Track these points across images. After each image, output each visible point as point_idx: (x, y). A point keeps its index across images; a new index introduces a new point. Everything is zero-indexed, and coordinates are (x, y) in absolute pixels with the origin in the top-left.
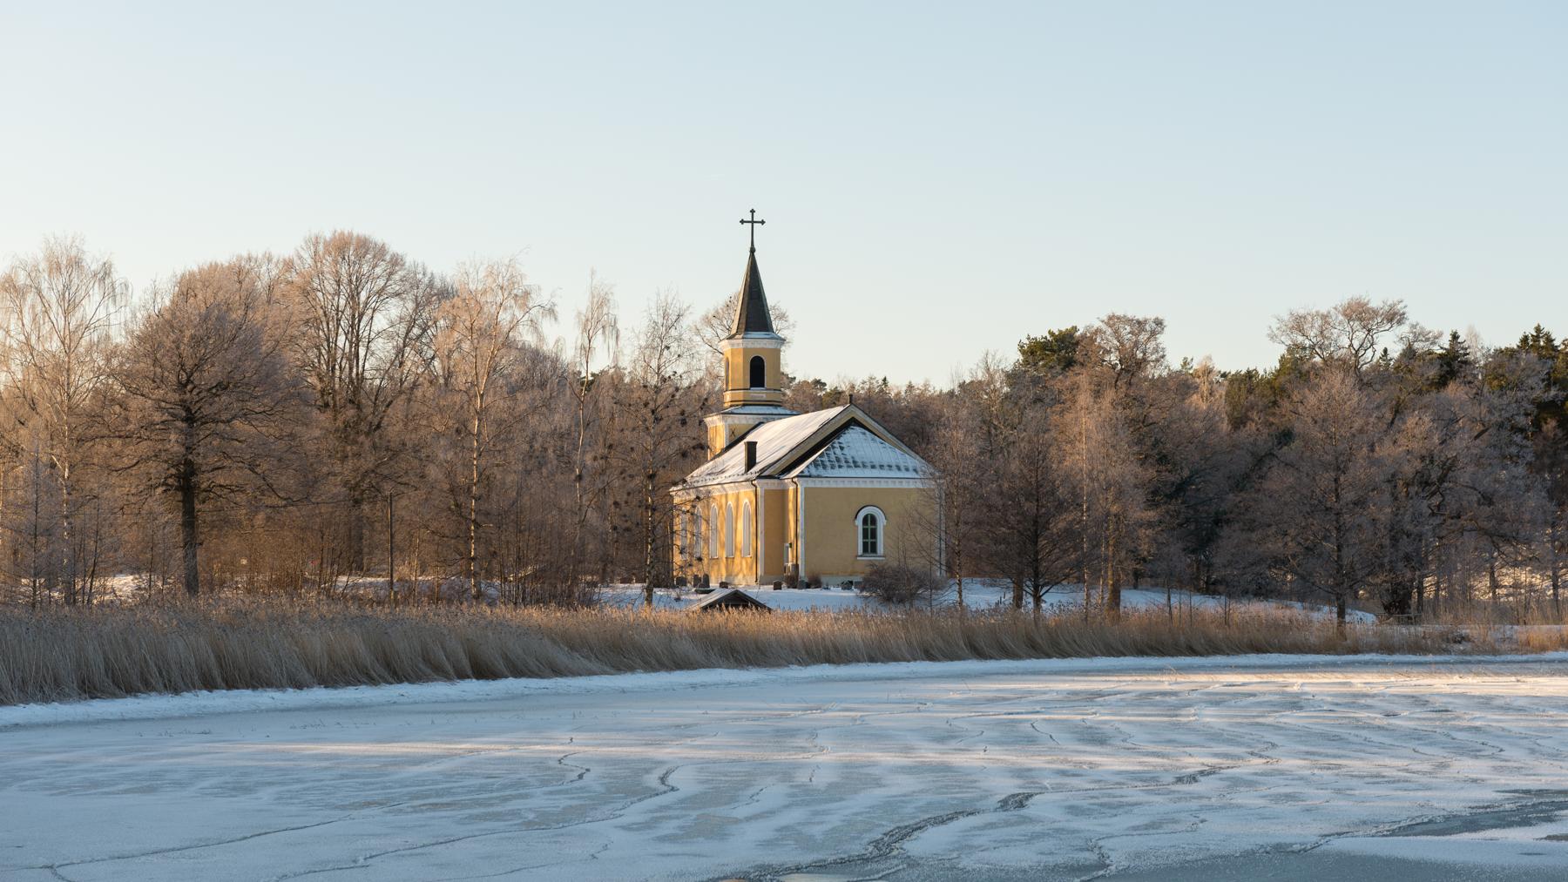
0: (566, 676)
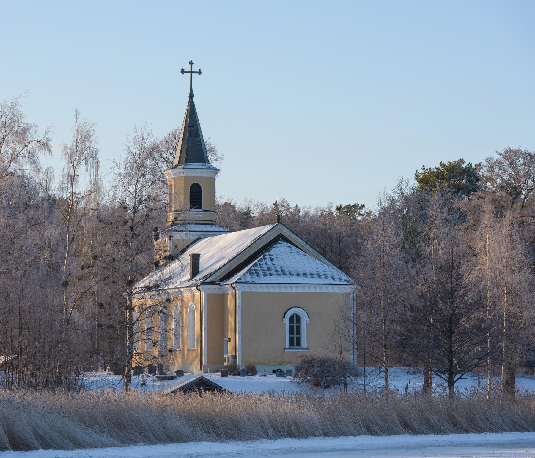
0: (85, 448)
